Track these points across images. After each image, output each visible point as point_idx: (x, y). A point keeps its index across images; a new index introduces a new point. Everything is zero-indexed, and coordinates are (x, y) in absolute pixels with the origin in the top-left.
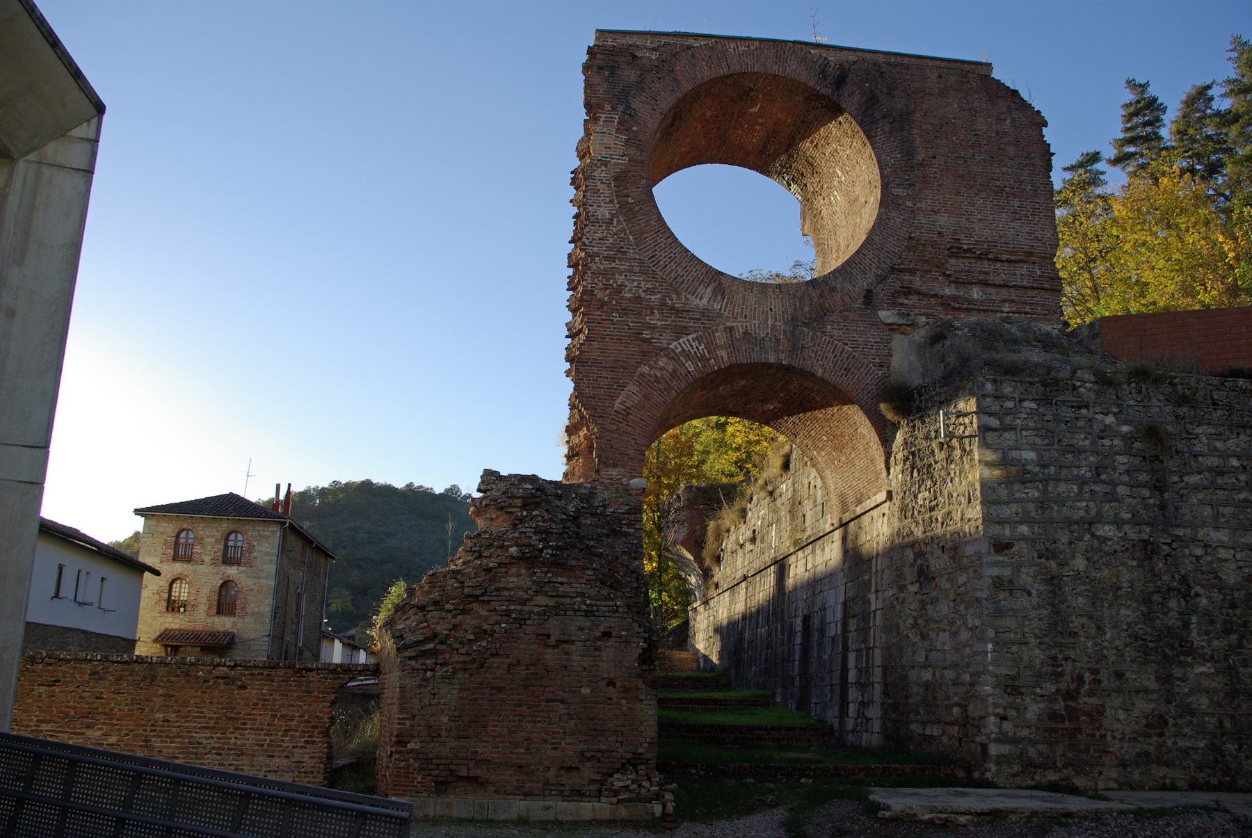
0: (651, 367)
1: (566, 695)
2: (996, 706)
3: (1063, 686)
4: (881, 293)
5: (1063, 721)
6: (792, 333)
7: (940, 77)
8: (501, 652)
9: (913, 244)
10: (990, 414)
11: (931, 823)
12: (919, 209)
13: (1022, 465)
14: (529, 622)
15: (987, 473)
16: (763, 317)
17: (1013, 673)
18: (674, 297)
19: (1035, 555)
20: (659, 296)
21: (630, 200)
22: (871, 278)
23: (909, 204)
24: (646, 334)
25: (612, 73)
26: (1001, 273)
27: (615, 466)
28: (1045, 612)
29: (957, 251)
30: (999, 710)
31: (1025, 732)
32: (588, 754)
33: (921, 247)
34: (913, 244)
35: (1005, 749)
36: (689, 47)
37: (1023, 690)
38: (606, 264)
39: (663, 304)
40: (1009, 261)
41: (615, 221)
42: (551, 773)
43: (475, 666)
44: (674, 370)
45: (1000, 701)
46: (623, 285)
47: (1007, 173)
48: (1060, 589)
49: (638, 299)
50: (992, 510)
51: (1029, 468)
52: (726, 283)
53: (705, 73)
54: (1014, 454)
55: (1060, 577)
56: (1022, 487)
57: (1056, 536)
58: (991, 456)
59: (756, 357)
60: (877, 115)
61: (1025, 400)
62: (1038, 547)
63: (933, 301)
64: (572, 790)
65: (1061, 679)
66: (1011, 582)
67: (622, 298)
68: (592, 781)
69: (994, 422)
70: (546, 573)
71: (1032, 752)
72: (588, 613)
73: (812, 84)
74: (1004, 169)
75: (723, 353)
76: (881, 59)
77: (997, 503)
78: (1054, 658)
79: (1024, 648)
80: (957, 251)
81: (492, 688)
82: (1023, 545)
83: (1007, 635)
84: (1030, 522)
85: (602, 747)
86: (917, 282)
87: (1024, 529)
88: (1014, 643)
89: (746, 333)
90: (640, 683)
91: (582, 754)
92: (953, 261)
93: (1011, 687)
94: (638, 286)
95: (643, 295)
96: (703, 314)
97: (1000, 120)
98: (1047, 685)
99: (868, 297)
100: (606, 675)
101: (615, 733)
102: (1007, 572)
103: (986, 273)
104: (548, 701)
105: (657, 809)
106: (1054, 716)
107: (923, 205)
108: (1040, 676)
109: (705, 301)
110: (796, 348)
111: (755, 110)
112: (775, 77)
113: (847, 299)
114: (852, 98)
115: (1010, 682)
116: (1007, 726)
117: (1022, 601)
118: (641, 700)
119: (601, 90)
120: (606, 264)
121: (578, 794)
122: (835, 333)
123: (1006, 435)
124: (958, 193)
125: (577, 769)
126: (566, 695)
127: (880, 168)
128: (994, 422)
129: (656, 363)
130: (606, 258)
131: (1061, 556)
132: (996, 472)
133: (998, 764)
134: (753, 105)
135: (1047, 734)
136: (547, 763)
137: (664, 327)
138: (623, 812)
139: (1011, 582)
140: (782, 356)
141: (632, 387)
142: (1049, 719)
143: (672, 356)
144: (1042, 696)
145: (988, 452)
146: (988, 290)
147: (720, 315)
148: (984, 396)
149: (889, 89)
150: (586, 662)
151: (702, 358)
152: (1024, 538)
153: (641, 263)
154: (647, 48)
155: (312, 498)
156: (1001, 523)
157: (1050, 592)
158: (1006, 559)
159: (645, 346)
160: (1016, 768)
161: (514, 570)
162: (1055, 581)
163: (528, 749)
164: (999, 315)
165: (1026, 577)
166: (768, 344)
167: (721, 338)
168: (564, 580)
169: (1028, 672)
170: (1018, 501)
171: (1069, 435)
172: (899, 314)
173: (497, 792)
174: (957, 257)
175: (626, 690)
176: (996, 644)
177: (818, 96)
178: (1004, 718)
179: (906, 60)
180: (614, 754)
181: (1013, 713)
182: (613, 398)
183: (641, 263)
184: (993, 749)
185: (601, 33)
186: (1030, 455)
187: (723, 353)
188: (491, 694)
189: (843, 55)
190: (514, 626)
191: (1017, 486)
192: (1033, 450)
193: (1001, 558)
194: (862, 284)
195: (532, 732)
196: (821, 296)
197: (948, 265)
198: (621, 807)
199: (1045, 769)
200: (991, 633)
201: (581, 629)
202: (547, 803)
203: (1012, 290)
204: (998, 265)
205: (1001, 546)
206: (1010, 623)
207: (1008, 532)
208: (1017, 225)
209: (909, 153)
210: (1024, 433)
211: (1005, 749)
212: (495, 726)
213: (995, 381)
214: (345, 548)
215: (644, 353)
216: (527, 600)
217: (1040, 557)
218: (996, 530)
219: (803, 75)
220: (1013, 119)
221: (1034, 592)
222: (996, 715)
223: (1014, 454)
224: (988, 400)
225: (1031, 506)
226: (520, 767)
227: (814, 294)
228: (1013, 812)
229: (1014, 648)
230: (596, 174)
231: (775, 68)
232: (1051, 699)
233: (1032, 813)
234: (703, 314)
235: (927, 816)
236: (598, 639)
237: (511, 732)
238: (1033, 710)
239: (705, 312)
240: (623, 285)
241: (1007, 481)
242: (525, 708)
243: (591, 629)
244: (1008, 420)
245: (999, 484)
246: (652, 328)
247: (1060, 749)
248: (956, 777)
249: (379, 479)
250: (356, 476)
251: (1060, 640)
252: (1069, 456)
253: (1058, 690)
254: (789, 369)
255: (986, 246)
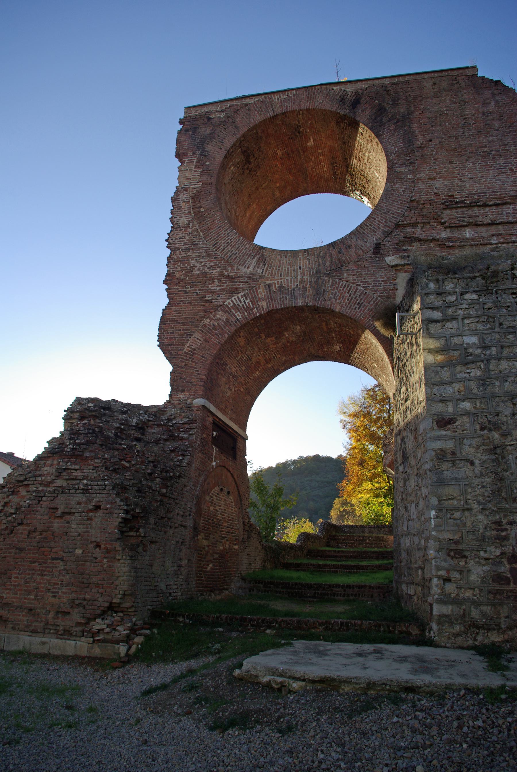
0: (211, 319)
1: (65, 555)
2: (438, 568)
3: (508, 549)
4: (388, 244)
5: (509, 583)
6: (316, 282)
7: (434, 84)
8: (25, 521)
9: (413, 204)
10: (433, 309)
11: (268, 686)
12: (418, 179)
13: (465, 349)
14: (44, 499)
15: (430, 358)
16: (294, 274)
17: (457, 537)
18: (229, 269)
19: (478, 427)
20: (218, 270)
21: (202, 210)
22: (379, 234)
23: (410, 176)
24: (209, 297)
25: (194, 132)
26: (489, 215)
27: (183, 391)
28: (488, 480)
29: (451, 204)
30: (442, 573)
31: (468, 594)
32: (77, 602)
33: (421, 206)
34: (413, 204)
35: (447, 609)
36: (246, 105)
37: (467, 554)
38: (184, 254)
39: (221, 275)
40: (497, 205)
41: (191, 225)
42: (51, 615)
43: (7, 532)
44: (227, 320)
45: (443, 564)
46: (194, 266)
47: (493, 141)
48: (503, 457)
49: (204, 274)
50: (435, 390)
51: (471, 350)
52: (266, 254)
53: (257, 118)
54: (456, 340)
55: (503, 447)
56: (464, 368)
57: (499, 409)
58: (433, 344)
59: (287, 303)
60: (385, 120)
61: (466, 293)
62: (481, 420)
63: (432, 245)
64: (64, 630)
65: (505, 542)
66: (453, 453)
67: (193, 275)
68: (79, 624)
69: (437, 315)
70: (67, 462)
71: (475, 613)
72: (85, 491)
73: (334, 109)
74: (490, 139)
75: (263, 304)
76: (387, 81)
77: (440, 384)
78: (498, 523)
79: (467, 513)
80: (451, 204)
81: (17, 549)
82: (466, 419)
83: (450, 502)
84: (472, 399)
85: (87, 596)
86: (418, 232)
87: (467, 405)
88: (457, 509)
89: (281, 287)
90: (118, 546)
91: (73, 601)
92: (448, 212)
93: (455, 551)
94: (205, 266)
95: (208, 270)
96: (250, 278)
97: (485, 104)
98: (492, 548)
99: (377, 248)
100: (93, 539)
101: (97, 585)
102: (450, 445)
103: (476, 216)
104: (53, 559)
105: (123, 649)
106: (499, 578)
107: (422, 175)
108: (483, 540)
109: (251, 269)
110: (319, 292)
111: (311, 143)
112: (308, 110)
113: (360, 252)
114: (363, 114)
115: (453, 546)
116: (450, 588)
117: (465, 471)
118: (119, 560)
119: (186, 145)
120: (184, 254)
121: (67, 634)
122: (351, 278)
123: (449, 325)
124: (451, 162)
125: (68, 613)
126: (65, 555)
127: (387, 156)
128: (437, 315)
129: (214, 316)
130: (183, 250)
131: (504, 427)
132: (439, 358)
133: (439, 623)
134: (307, 140)
135: (491, 596)
136: (48, 608)
137: (221, 291)
138: (97, 651)
139: (453, 453)
140: (308, 300)
141: (197, 335)
142: (494, 581)
143: (227, 310)
144: (486, 559)
145: (431, 341)
146: (479, 229)
147: (261, 277)
148: (427, 294)
149: (393, 100)
150: (81, 529)
151: (248, 309)
152: (467, 413)
153: (208, 250)
154: (217, 111)
155: (289, 465)
156: (444, 401)
157: (493, 461)
158: (449, 433)
159: (207, 305)
160: (458, 628)
161: (49, 462)
162: (498, 451)
163: (36, 596)
164: (489, 246)
165: (468, 449)
166: (297, 293)
167: (262, 292)
168: (77, 467)
169: (471, 537)
170: (461, 380)
171: (510, 318)
172: (401, 257)
173: (13, 628)
174: (451, 209)
175: (108, 551)
176: (439, 510)
177: (344, 117)
178: (447, 580)
179: (406, 79)
180: (96, 602)
181: (457, 575)
182: (183, 344)
183: (208, 250)
184: (437, 609)
185: (187, 108)
186: (474, 340)
187: (263, 304)
188: (15, 553)
189: (358, 86)
190: (34, 502)
191: (459, 368)
192: (475, 335)
193: (443, 433)
194: (372, 240)
195: (40, 583)
196: (340, 252)
197: (443, 216)
198: (96, 645)
199: (489, 630)
200: (434, 501)
201: (79, 503)
202: (44, 640)
203: (500, 227)
204: (487, 209)
205: (444, 422)
206: (452, 490)
207: (450, 409)
208: (503, 177)
209: (409, 140)
210: (466, 321)
211: (447, 609)
212: (17, 577)
213: (437, 281)
214: (306, 490)
215: (206, 311)
216: (50, 482)
217: (482, 429)
218: (439, 407)
219: (328, 105)
220: (497, 101)
221: (477, 462)
222: (439, 577)
223: (456, 340)
224: (432, 297)
225: (473, 385)
226: (31, 610)
227: (334, 252)
228: (347, 681)
229: (457, 515)
230: (180, 197)
231: (307, 105)
232: (496, 562)
233: (368, 684)
234: (250, 278)
235: (265, 679)
236: (91, 511)
237: (26, 582)
238: (477, 572)
239: (251, 277)
240: (194, 266)
241: (448, 364)
242: (36, 564)
243: (86, 503)
244: (450, 312)
245: (442, 367)
246: (213, 292)
247: (504, 611)
248: (409, 634)
249: (323, 453)
250: (309, 452)
251: (504, 505)
252: (511, 337)
253: (502, 554)
254: (315, 309)
255: (476, 197)
